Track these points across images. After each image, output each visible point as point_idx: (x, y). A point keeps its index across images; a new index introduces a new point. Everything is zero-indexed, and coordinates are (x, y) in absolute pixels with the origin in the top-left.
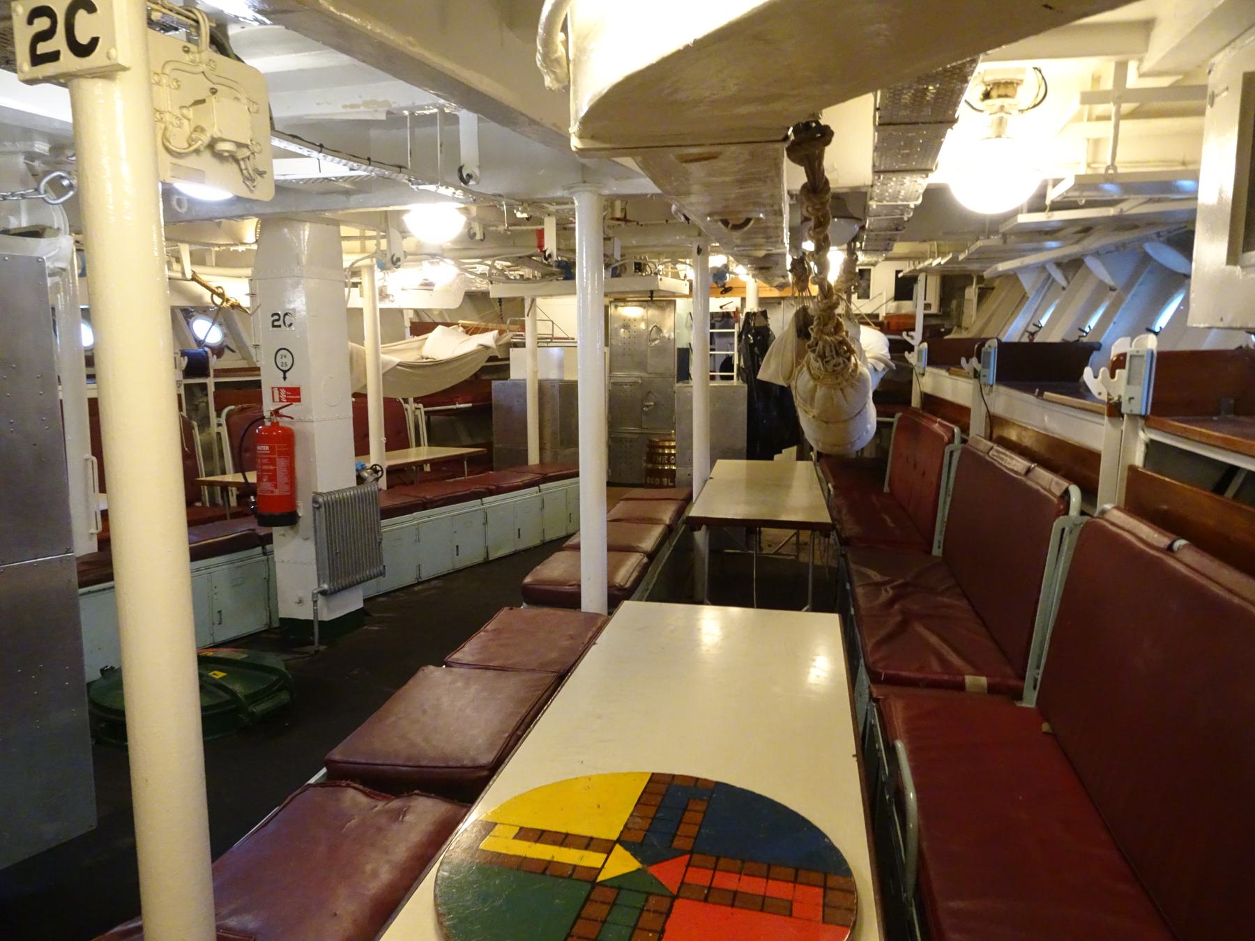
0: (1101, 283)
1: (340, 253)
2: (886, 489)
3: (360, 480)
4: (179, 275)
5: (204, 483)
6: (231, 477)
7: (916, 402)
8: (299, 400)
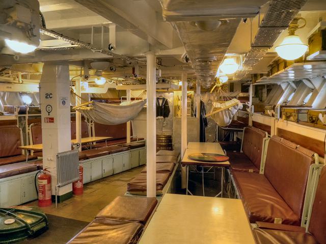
0: (310, 88)
1: (69, 76)
2: (241, 151)
3: (73, 148)
4: (18, 82)
5: (23, 149)
6: (31, 147)
7: (250, 124)
8: (53, 122)
